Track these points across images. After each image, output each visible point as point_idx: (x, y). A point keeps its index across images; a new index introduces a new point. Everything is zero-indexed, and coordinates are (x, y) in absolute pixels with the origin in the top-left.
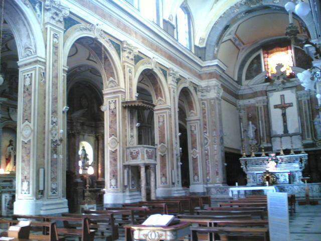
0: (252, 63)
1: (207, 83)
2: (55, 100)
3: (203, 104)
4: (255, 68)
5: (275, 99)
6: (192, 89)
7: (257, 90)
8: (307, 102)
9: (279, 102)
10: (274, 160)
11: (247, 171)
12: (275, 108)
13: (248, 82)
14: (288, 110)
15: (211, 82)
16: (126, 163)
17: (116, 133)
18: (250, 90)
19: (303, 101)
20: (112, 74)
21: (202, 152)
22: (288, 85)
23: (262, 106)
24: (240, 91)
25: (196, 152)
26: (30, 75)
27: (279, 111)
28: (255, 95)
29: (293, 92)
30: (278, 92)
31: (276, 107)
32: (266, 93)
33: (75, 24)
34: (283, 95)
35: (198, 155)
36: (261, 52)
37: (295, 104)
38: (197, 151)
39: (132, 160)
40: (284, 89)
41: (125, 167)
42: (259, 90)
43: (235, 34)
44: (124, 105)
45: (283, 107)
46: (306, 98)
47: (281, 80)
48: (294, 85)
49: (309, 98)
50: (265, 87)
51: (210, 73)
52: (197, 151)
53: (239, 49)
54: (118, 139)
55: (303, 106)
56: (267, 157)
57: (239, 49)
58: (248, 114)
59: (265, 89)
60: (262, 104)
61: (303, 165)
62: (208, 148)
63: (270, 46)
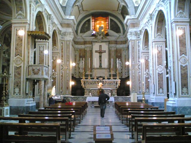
1: (65, 30)
3: (62, 43)
4: (86, 28)
5: (96, 47)
6: (57, 32)
7: (87, 40)
8: (114, 51)
9: (98, 49)
10: (102, 82)
11: (85, 87)
12: (96, 52)
13: (81, 34)
14: (103, 55)
15: (68, 30)
16: (29, 77)
17: (186, 53)
18: (82, 39)
19: (112, 50)
20: (21, 9)
21: (59, 74)
22: (105, 40)
24: (76, 39)
25: (146, 75)
27: (98, 54)
28: (85, 43)
29: (106, 44)
30: (99, 43)
31: (96, 52)
32: (91, 43)
34: (101, 45)
35: (57, 76)
36: (91, 18)
38: (145, 75)
40: (102, 42)
41: (27, 79)
42: (88, 40)
43: (81, 3)
44: (29, 34)
45: (100, 52)
46: (114, 49)
47: (102, 36)
48: (108, 41)
49: (115, 49)
50: (92, 39)
51: (67, 24)
53: (80, 13)
54: (22, 58)
55: (112, 53)
56: (98, 80)
57: (80, 13)
58: (80, 54)
59: (91, 40)
61: (118, 86)
62: (63, 72)
63: (96, 16)
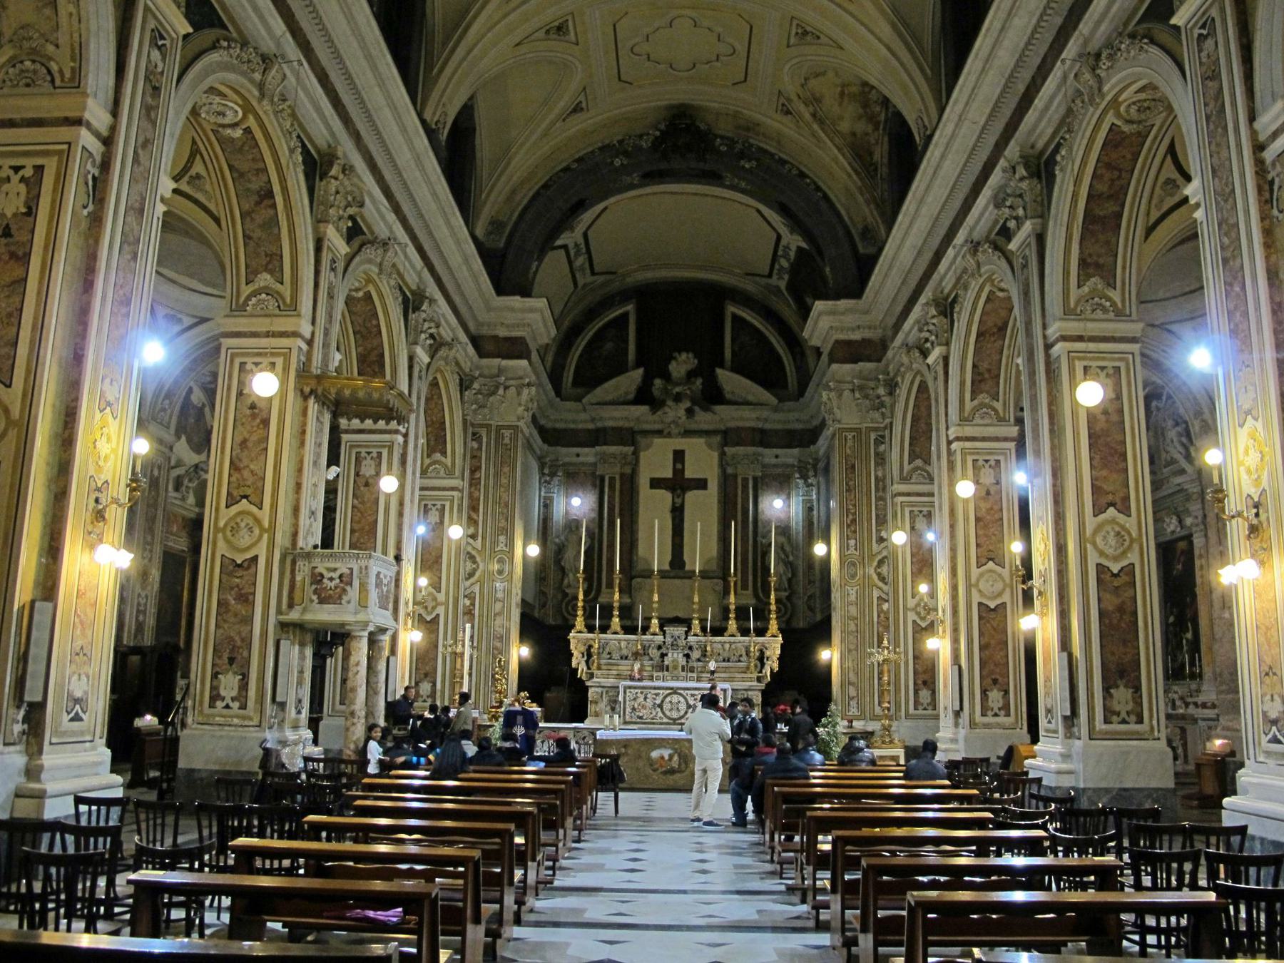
0: (600, 336)
2: (1228, 227)
11: (592, 676)
23: (617, 477)
26: (28, 172)
27: (665, 497)
33: (212, 26)
37: (713, 486)
39: (316, 605)
40: (688, 433)
52: (912, 616)
60: (617, 469)
62: (477, 589)
